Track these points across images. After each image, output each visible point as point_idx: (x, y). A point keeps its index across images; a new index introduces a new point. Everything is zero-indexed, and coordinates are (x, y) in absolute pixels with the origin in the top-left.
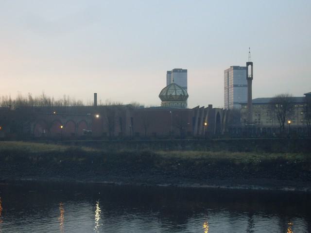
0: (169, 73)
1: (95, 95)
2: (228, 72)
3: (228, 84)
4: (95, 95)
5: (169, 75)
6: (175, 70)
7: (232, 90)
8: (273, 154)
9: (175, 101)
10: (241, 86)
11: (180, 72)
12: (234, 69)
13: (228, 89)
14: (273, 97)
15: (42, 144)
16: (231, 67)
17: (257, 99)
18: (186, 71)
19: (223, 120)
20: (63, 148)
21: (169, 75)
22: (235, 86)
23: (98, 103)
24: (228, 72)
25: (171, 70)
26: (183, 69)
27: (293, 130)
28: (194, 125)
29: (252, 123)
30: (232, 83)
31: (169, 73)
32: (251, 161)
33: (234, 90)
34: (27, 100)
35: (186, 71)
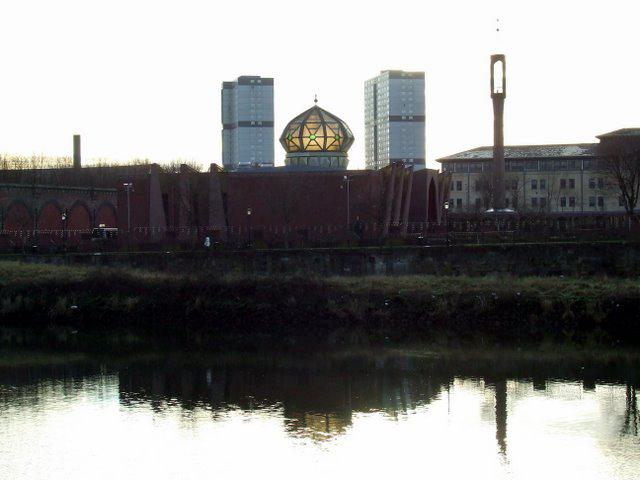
0: (227, 86)
1: (77, 139)
2: (375, 86)
4: (77, 139)
6: (243, 80)
7: (385, 130)
8: (627, 280)
11: (256, 84)
12: (390, 77)
13: (376, 127)
14: (126, 164)
15: (16, 264)
16: (383, 72)
17: (617, 132)
18: (269, 82)
19: (394, 201)
20: (79, 273)
23: (84, 163)
24: (375, 86)
25: (233, 78)
26: (264, 76)
30: (384, 112)
31: (227, 86)
32: (579, 298)
35: (269, 82)
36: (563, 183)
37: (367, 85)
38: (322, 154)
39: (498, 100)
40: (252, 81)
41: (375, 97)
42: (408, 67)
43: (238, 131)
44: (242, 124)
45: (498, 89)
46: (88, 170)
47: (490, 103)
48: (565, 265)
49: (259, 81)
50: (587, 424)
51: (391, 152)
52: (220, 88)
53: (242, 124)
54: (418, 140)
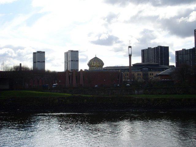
0: (34, 53)
3: (67, 60)
5: (34, 54)
6: (38, 52)
7: (70, 63)
13: (67, 63)
17: (137, 63)
18: (44, 52)
21: (34, 54)
22: (72, 61)
25: (35, 51)
27: (136, 65)
28: (70, 81)
29: (68, 116)
30: (70, 59)
31: (34, 53)
35: (44, 52)
36: (138, 74)
37: (65, 53)
41: (67, 57)
42: (75, 49)
43: (37, 63)
44: (38, 62)
46: (48, 73)
53: (38, 62)
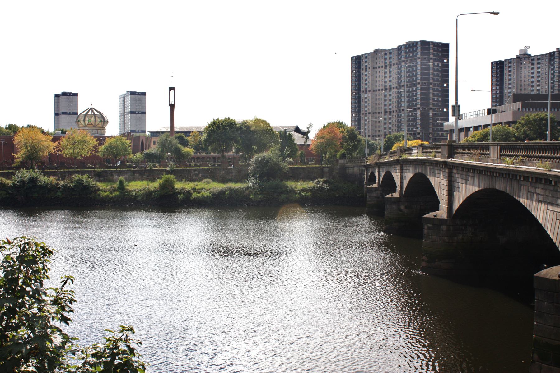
0: (57, 96)
2: (124, 98)
6: (64, 94)
9: (94, 127)
10: (138, 113)
11: (70, 95)
21: (56, 98)
23: (176, 129)
24: (124, 98)
25: (59, 93)
26: (74, 92)
30: (128, 109)
31: (57, 96)
33: (130, 116)
34: (340, 125)
38: (94, 128)
39: (172, 106)
40: (68, 94)
45: (172, 102)
47: (168, 108)
48: (194, 178)
49: (71, 94)
50: (372, 244)
51: (130, 127)
52: (54, 96)
54: (143, 122)
